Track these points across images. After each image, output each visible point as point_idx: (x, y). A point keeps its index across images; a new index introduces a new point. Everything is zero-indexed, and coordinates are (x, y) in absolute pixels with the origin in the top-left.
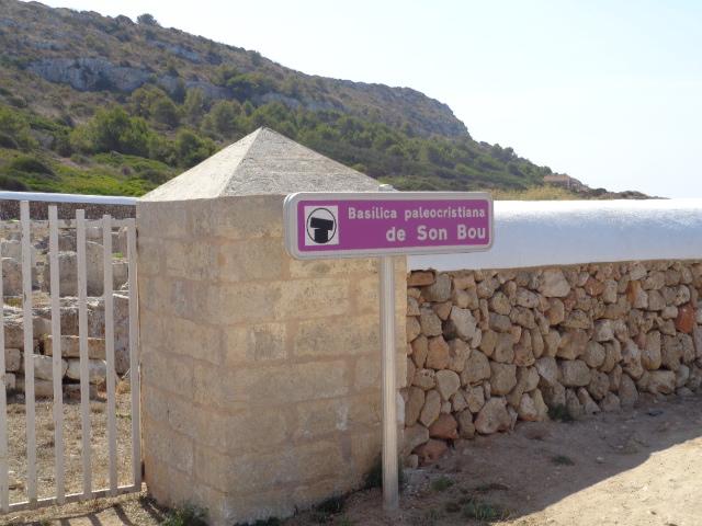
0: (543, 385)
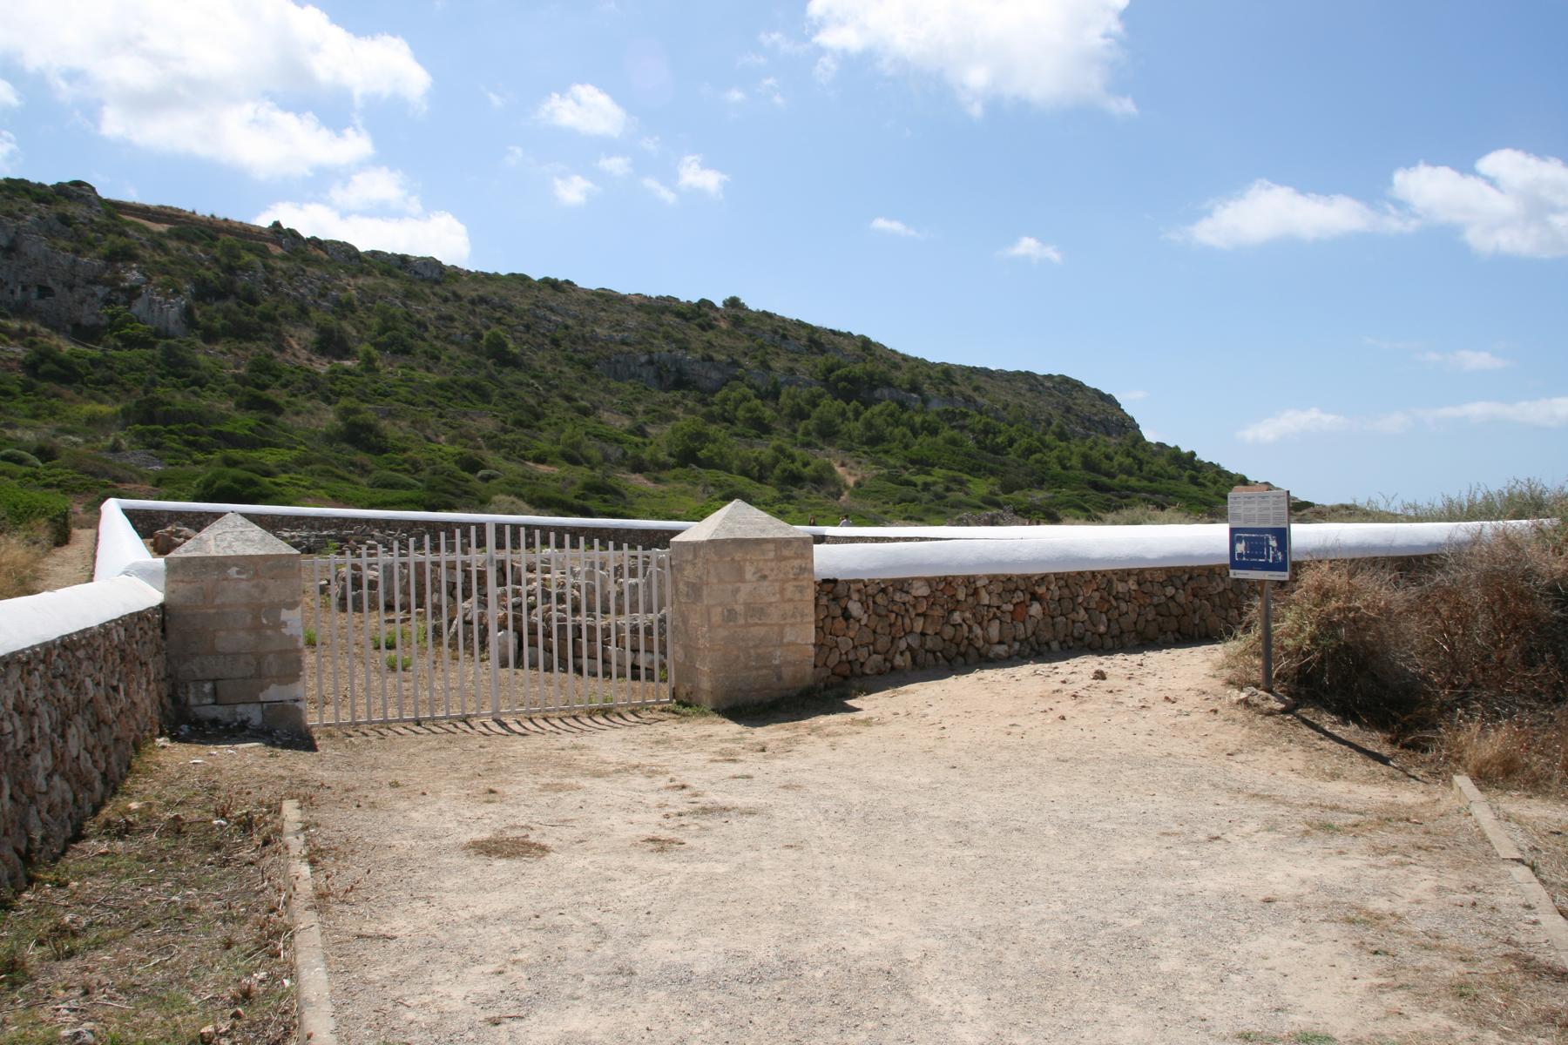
0: (909, 647)
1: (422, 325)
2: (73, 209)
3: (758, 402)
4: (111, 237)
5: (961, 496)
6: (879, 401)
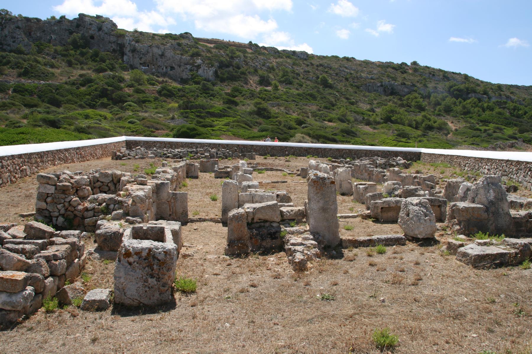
1: (298, 74)
2: (183, 41)
3: (421, 100)
4: (193, 49)
5: (500, 135)
6: (470, 98)
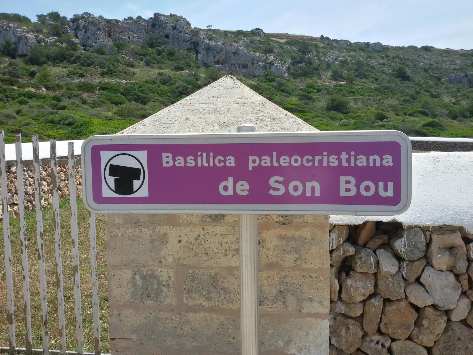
1: (373, 67)
